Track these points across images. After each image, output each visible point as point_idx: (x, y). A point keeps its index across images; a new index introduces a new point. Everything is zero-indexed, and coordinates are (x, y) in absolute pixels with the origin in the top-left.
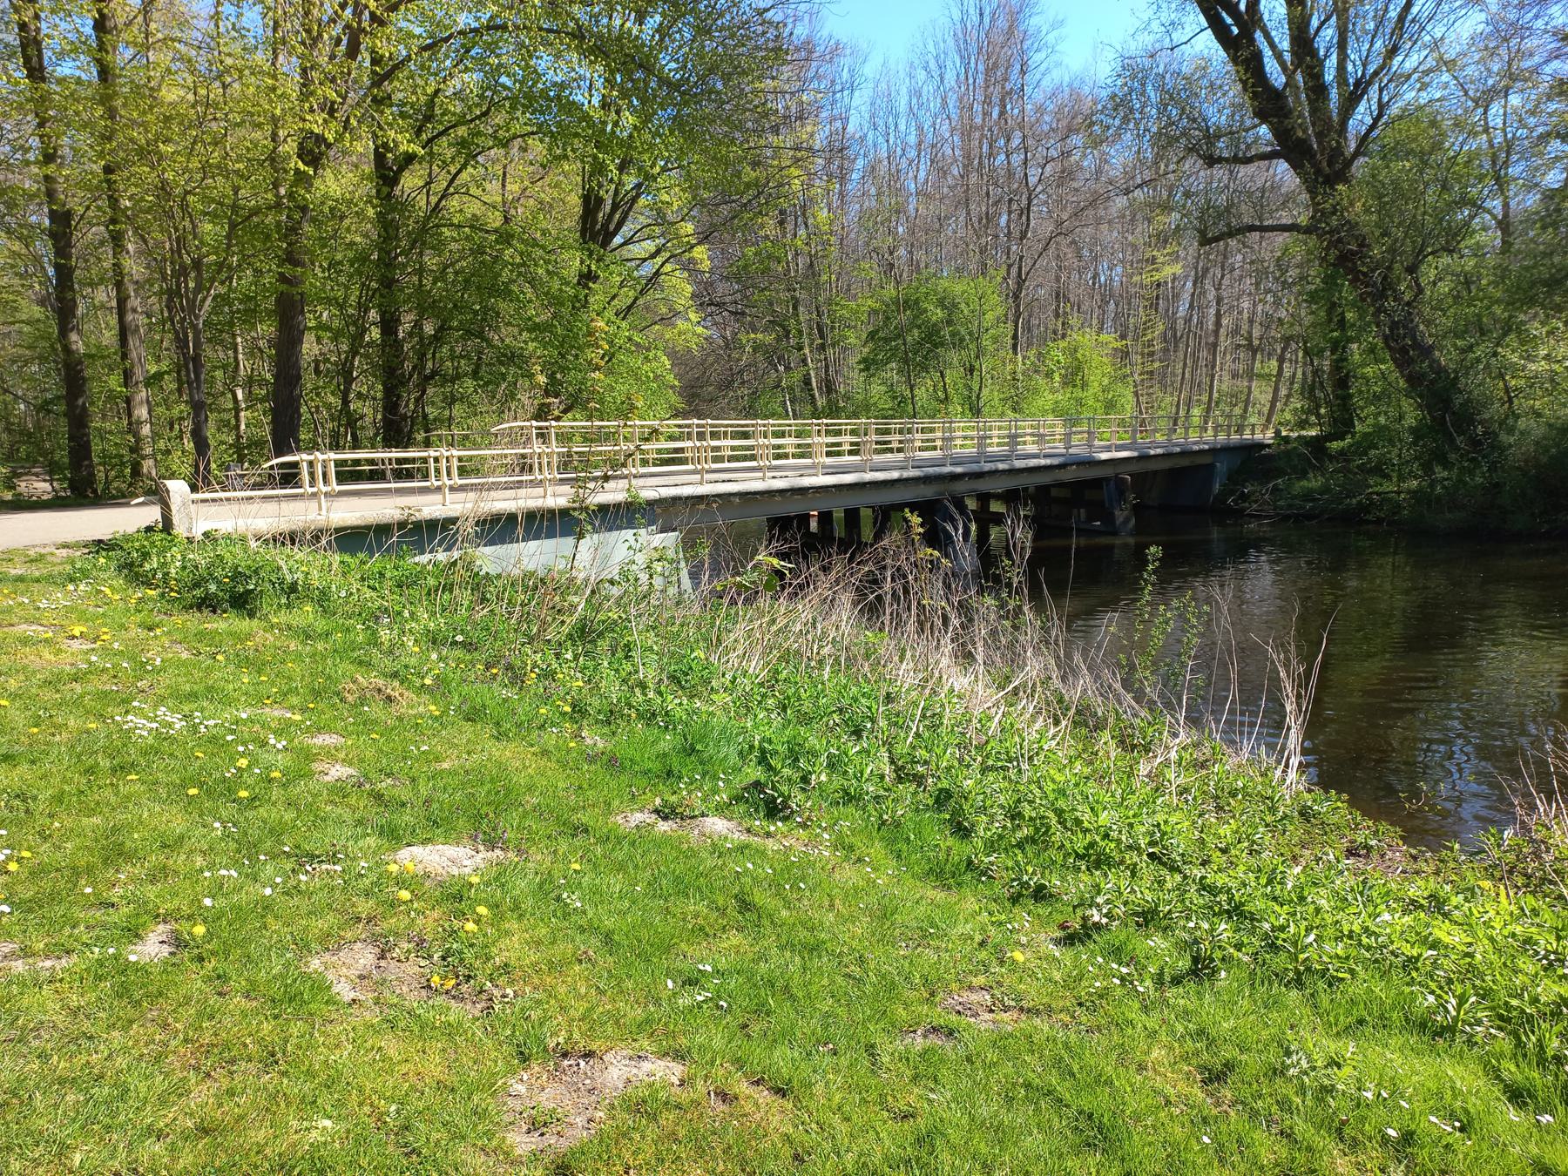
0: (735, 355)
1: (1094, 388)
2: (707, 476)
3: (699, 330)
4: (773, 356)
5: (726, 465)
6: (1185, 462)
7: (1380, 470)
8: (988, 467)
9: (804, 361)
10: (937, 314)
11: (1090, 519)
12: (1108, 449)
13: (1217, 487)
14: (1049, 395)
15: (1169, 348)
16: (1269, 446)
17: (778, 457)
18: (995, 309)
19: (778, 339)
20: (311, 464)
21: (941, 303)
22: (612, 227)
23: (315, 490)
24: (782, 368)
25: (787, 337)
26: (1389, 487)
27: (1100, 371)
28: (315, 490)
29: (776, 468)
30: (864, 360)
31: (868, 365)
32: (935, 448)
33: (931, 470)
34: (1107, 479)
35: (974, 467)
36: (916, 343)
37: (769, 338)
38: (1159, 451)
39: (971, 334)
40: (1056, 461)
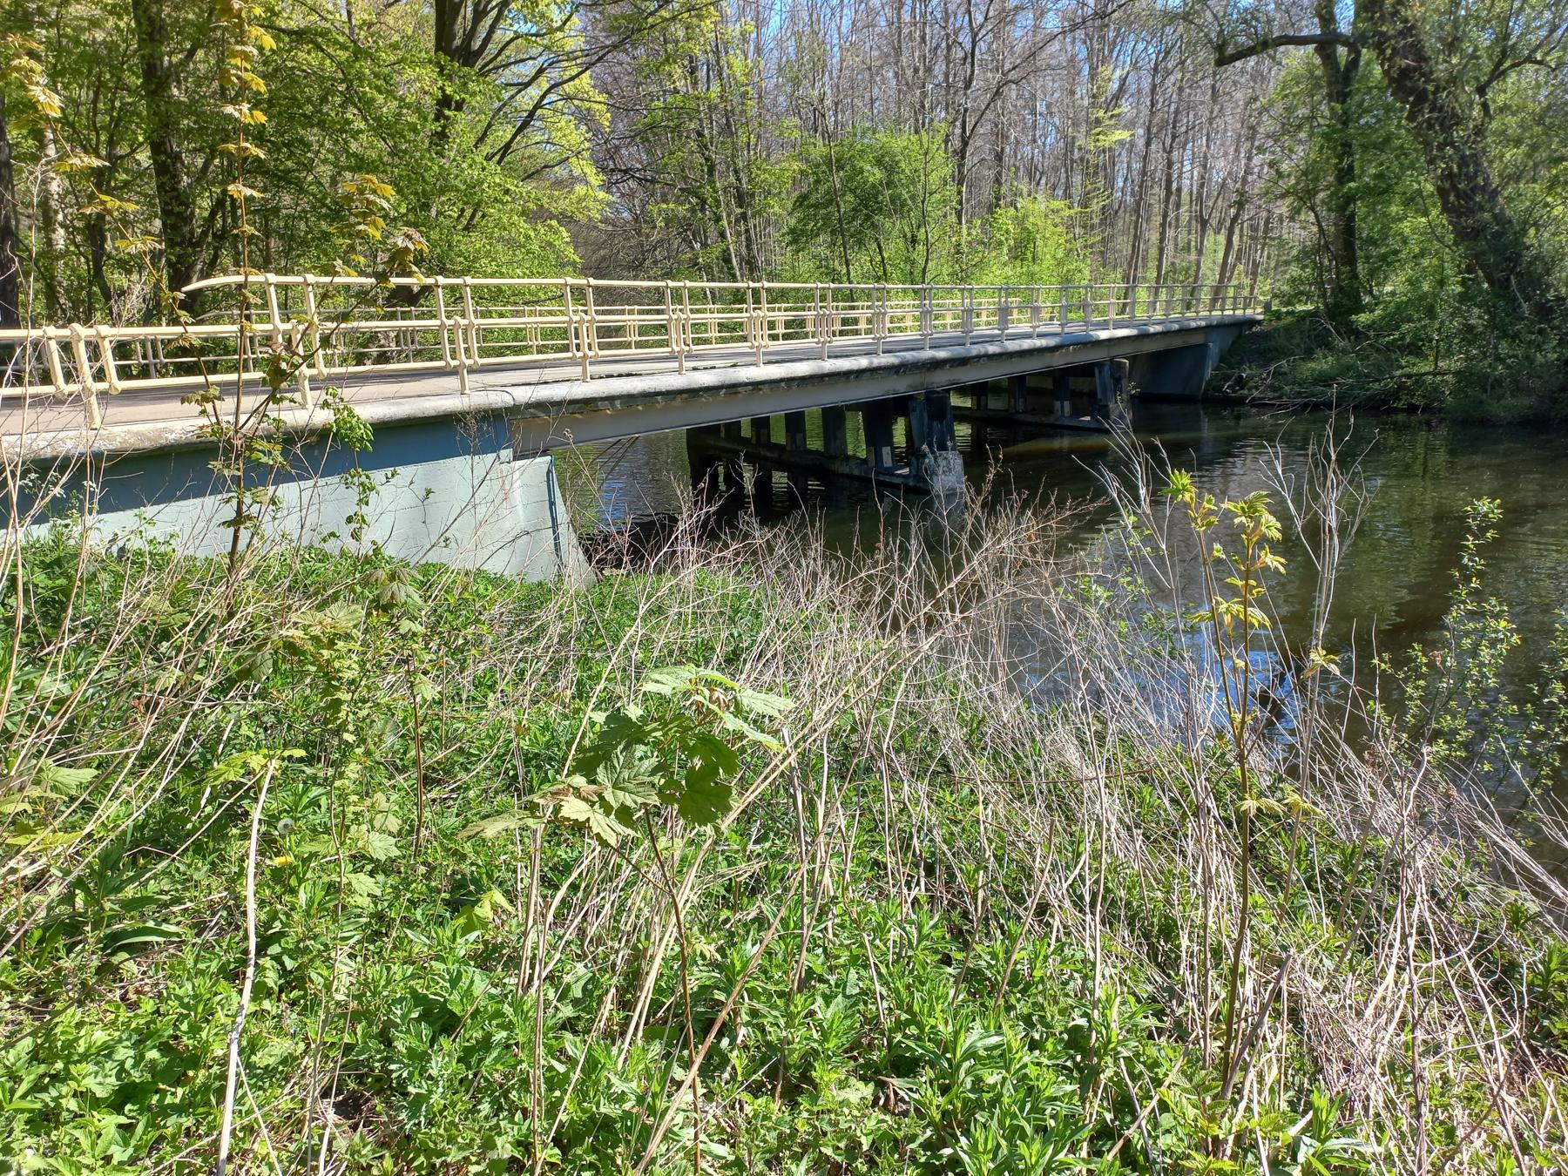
0: (646, 230)
1: (1048, 261)
2: (591, 369)
3: (602, 195)
4: (689, 230)
5: (535, 357)
6: (1177, 342)
7: (1414, 349)
8: (975, 350)
9: (722, 235)
10: (875, 175)
11: (1077, 413)
12: (1104, 325)
13: (1209, 373)
14: (999, 271)
15: (1119, 222)
16: (1259, 322)
17: (697, 341)
18: (941, 169)
19: (693, 211)
20: (66, 347)
21: (879, 162)
22: (476, 45)
23: (456, 363)
24: (697, 246)
25: (703, 210)
26: (1425, 367)
27: (1051, 245)
28: (73, 387)
29: (697, 357)
30: (792, 231)
31: (797, 238)
32: (857, 332)
33: (909, 356)
34: (1100, 365)
35: (959, 351)
36: (851, 210)
37: (682, 210)
38: (1158, 328)
39: (913, 198)
40: (1052, 342)
